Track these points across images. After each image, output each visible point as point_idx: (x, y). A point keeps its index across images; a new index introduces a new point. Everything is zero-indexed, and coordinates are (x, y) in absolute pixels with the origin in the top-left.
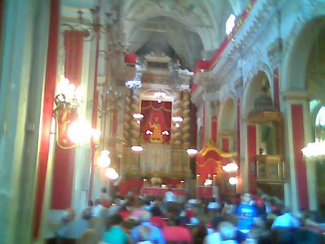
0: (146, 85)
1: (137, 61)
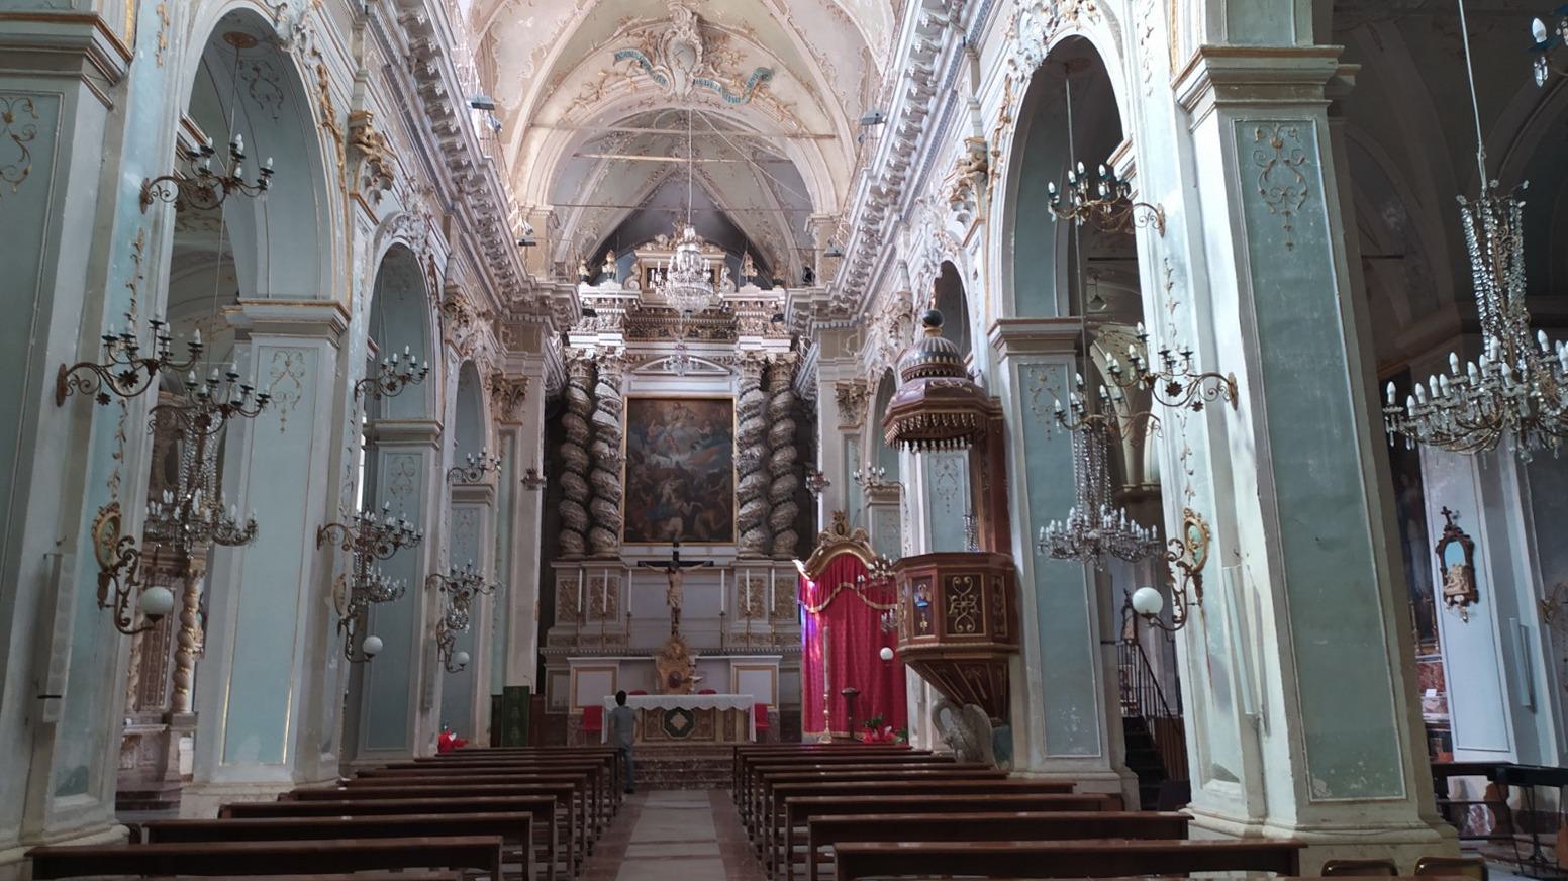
0: (641, 347)
1: (609, 259)
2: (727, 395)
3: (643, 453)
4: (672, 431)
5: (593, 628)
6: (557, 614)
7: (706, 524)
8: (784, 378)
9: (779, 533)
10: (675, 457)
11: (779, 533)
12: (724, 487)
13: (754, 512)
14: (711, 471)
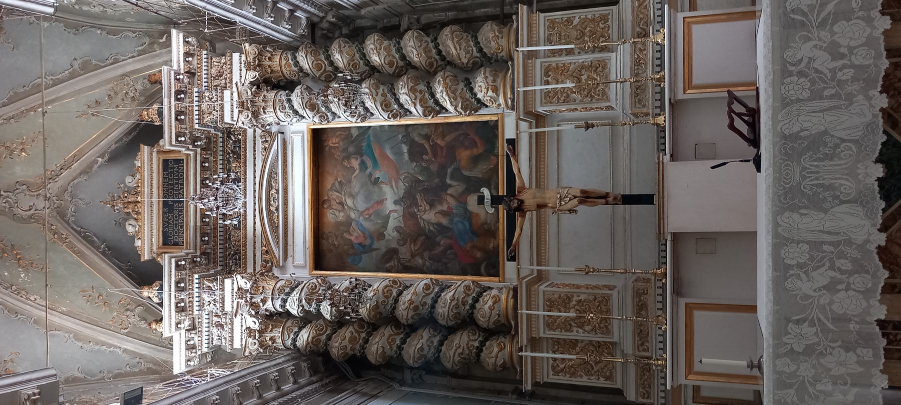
0: (253, 257)
2: (307, 137)
3: (384, 250)
4: (355, 209)
5: (622, 332)
6: (601, 383)
7: (475, 160)
8: (277, 59)
9: (480, 50)
10: (390, 205)
11: (480, 50)
12: (427, 137)
13: (446, 86)
14: (406, 157)
